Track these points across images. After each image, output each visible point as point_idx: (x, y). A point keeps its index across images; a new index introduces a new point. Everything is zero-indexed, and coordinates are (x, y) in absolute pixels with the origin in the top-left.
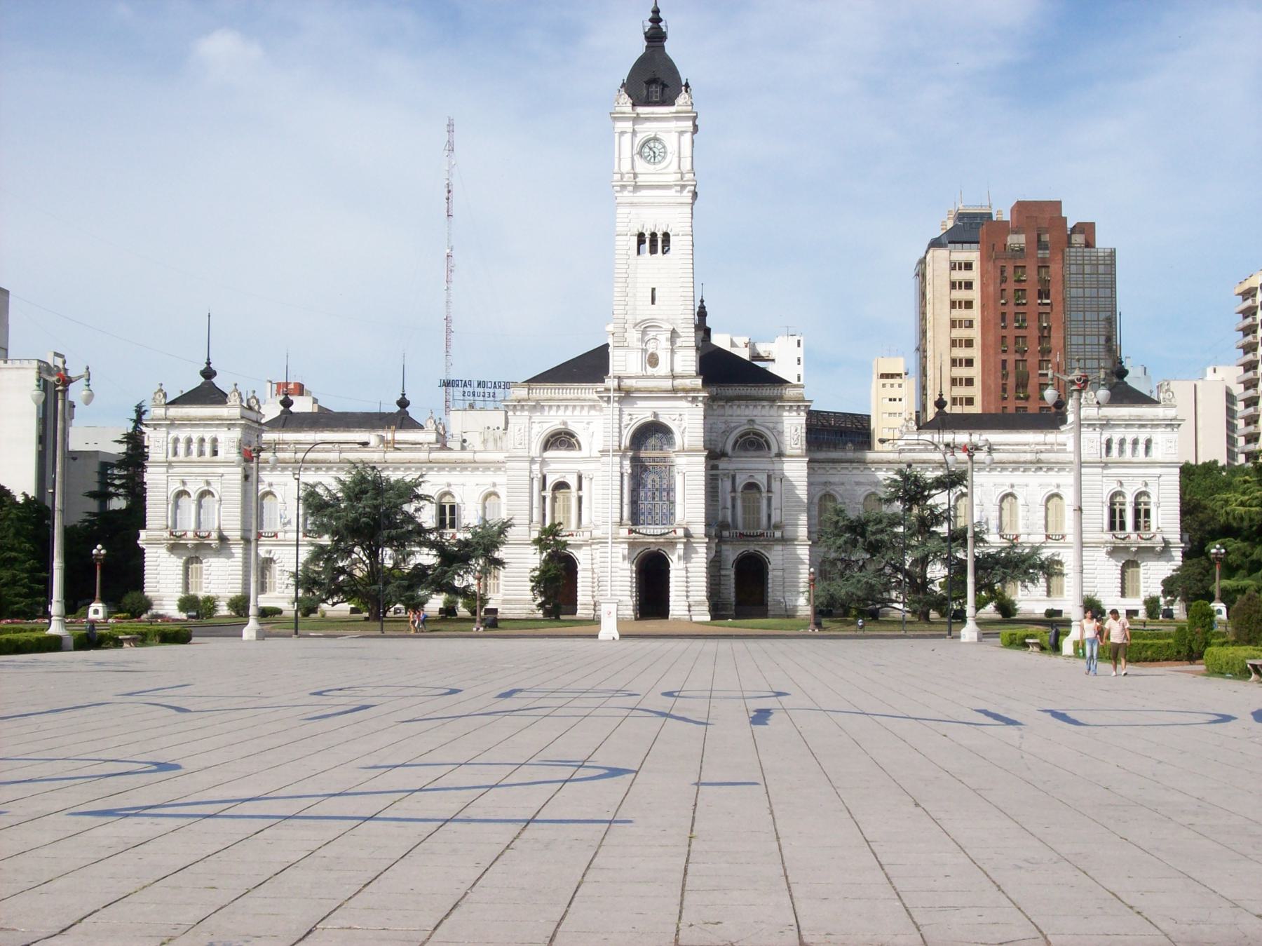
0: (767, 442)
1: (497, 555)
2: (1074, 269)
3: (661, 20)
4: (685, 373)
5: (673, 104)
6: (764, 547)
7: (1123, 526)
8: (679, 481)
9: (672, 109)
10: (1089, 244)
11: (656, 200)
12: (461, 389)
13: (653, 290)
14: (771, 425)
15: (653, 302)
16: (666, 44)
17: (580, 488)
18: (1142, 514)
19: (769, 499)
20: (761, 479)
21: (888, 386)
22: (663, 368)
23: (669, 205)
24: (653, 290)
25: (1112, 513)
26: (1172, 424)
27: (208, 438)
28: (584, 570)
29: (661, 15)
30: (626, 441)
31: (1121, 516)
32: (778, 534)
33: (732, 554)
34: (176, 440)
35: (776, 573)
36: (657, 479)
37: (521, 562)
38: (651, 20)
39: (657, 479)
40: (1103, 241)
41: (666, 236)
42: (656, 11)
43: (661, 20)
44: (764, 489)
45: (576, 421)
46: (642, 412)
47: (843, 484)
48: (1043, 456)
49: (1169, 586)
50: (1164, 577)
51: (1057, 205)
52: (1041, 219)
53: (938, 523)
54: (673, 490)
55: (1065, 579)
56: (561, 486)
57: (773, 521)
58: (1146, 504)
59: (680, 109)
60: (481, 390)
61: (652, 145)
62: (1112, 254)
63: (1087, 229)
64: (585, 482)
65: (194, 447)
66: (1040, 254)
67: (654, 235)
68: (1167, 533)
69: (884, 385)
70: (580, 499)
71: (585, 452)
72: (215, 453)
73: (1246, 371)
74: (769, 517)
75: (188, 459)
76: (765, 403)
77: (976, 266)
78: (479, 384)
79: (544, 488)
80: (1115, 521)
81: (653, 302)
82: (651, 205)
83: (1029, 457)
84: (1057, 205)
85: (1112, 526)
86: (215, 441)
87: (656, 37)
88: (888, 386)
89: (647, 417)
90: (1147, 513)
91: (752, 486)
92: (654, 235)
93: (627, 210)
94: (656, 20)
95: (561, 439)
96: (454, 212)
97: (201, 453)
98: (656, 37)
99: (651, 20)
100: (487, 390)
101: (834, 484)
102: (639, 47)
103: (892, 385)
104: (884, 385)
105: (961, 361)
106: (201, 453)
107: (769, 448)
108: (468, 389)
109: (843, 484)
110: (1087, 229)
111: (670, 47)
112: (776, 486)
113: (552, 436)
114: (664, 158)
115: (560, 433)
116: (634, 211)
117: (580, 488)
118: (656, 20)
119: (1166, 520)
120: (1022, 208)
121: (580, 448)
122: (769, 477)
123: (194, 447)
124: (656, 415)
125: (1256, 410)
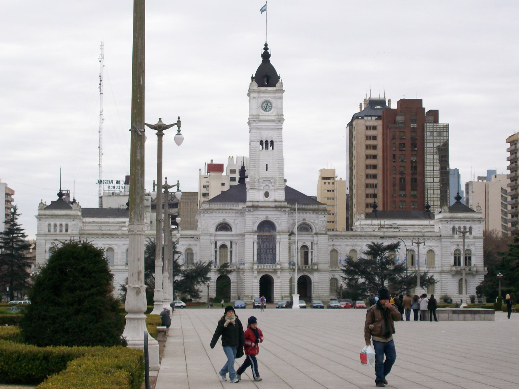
0: (311, 228)
1: (208, 276)
2: (428, 134)
3: (268, 49)
4: (280, 200)
5: (275, 86)
6: (310, 273)
7: (459, 264)
8: (278, 246)
9: (274, 88)
10: (436, 121)
11: (267, 127)
12: (107, 185)
13: (267, 165)
14: (313, 221)
15: (267, 170)
16: (270, 59)
17: (231, 247)
18: (468, 259)
19: (312, 252)
20: (309, 244)
21: (327, 184)
22: (271, 198)
23: (273, 129)
24: (267, 165)
25: (455, 258)
26: (480, 220)
27: (64, 224)
28: (233, 282)
29: (268, 47)
30: (255, 228)
31: (466, 262)
32: (316, 267)
33: (296, 277)
34: (49, 225)
35: (315, 284)
36: (268, 245)
37: (213, 276)
38: (264, 49)
39: (268, 245)
40: (442, 120)
41: (272, 142)
42: (266, 45)
43: (268, 49)
44: (310, 248)
45: (229, 218)
46: (262, 216)
47: (340, 245)
48: (426, 234)
49: (479, 290)
50: (477, 286)
51: (420, 101)
52: (412, 108)
53: (389, 264)
54: (275, 249)
55: (436, 285)
56: (223, 246)
57: (313, 262)
58: (469, 254)
59: (277, 88)
60: (118, 185)
61: (269, 104)
62: (447, 127)
63: (434, 114)
64: (234, 246)
65: (58, 229)
66: (412, 126)
67: (267, 141)
68: (479, 267)
69: (325, 183)
70: (231, 252)
71: (234, 232)
72: (67, 231)
73: (512, 181)
74: (312, 260)
75: (55, 233)
76: (310, 212)
77: (380, 128)
78: (117, 182)
79: (216, 247)
80: (457, 262)
81: (267, 170)
82: (266, 129)
83: (420, 234)
84: (420, 101)
85: (455, 264)
86: (67, 225)
87: (266, 56)
88: (327, 184)
89: (262, 218)
90: (470, 258)
91: (304, 247)
92: (267, 141)
93: (256, 131)
94: (266, 48)
95: (224, 227)
96: (103, 91)
97: (61, 231)
98: (266, 56)
99: (264, 49)
100: (121, 185)
101: (337, 245)
102: (260, 61)
103: (329, 183)
104: (325, 183)
105: (370, 175)
106: (61, 231)
107: (312, 231)
108: (111, 185)
109: (340, 245)
110: (434, 114)
111: (273, 60)
112: (315, 247)
113: (219, 225)
114: (271, 109)
115: (222, 224)
116: (258, 131)
117: (231, 247)
118: (266, 48)
119: (478, 260)
120: (402, 103)
121: (231, 230)
122: (312, 243)
123: (58, 229)
124: (267, 217)
125: (516, 174)
